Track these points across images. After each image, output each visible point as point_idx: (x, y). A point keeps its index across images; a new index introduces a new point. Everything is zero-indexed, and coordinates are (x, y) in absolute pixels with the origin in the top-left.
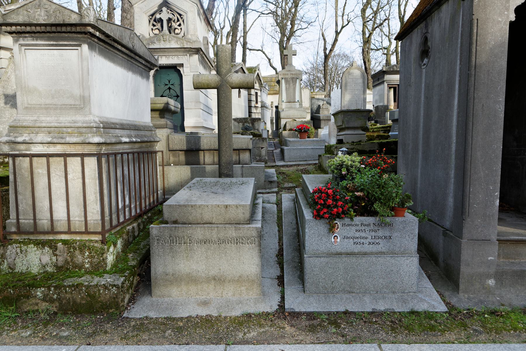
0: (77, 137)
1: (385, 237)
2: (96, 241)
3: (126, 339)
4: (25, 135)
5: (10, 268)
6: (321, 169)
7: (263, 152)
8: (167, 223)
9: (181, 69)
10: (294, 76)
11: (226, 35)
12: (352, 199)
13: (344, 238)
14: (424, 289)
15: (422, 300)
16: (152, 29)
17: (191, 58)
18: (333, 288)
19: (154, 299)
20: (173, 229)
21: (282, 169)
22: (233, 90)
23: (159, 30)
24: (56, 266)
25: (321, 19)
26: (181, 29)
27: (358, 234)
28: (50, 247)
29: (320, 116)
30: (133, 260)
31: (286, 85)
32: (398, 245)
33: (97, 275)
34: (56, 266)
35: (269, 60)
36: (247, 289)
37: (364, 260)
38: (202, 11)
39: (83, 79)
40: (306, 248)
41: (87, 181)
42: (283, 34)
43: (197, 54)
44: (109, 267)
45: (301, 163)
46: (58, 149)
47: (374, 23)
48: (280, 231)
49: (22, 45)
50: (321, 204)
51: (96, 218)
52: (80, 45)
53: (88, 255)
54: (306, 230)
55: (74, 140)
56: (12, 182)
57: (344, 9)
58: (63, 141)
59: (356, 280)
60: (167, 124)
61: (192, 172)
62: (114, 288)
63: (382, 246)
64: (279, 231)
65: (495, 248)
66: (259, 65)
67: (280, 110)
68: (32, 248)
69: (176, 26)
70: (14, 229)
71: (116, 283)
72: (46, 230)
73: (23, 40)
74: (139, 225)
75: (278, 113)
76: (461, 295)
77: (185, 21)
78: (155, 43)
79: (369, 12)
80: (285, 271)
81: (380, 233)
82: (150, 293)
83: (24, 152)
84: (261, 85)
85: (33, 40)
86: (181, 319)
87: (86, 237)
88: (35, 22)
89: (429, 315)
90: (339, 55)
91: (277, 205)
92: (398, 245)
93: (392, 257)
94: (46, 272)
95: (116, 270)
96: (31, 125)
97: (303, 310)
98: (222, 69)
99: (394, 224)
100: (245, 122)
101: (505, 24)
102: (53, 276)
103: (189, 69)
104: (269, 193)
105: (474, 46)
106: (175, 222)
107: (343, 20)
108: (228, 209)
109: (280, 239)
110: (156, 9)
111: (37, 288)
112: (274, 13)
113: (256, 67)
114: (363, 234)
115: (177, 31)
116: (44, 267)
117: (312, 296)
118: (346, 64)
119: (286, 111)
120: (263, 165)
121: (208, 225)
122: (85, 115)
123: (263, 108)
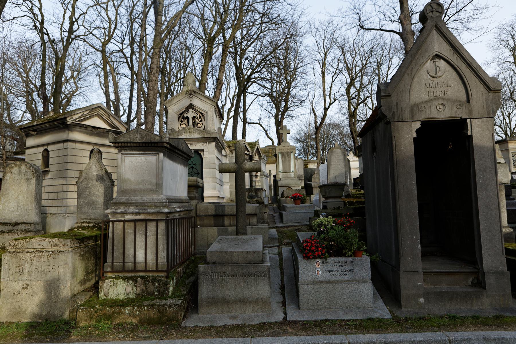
0: (154, 209)
1: (350, 270)
2: (163, 277)
3: (186, 337)
4: (122, 208)
5: (105, 295)
6: (311, 228)
7: (266, 216)
8: (209, 264)
9: (202, 153)
10: (288, 151)
11: (227, 111)
12: (328, 246)
13: (324, 271)
14: (378, 306)
15: (376, 312)
16: (181, 124)
17: (210, 145)
18: (318, 306)
19: (200, 315)
20: (214, 267)
21: (281, 229)
22: (246, 173)
23: (186, 125)
25: (311, 97)
26: (202, 124)
27: (332, 269)
28: (133, 281)
29: (312, 184)
30: (184, 290)
31: (282, 158)
32: (359, 276)
33: (163, 299)
35: (266, 131)
36: (261, 308)
37: (337, 286)
38: (217, 110)
39: (159, 173)
40: (300, 279)
41: (159, 237)
42: (278, 108)
43: (214, 142)
44: (170, 295)
45: (297, 224)
47: (358, 100)
48: (282, 273)
49: (123, 154)
50: (308, 250)
52: (158, 154)
54: (299, 267)
55: (153, 211)
57: (331, 90)
58: (146, 212)
59: (333, 300)
60: (195, 197)
61: (218, 232)
62: (176, 306)
63: (348, 276)
64: (281, 273)
65: (422, 277)
66: (258, 140)
67: (277, 179)
69: (199, 122)
70: (109, 269)
71: (177, 303)
72: (130, 269)
73: (124, 151)
74: (183, 269)
75: (275, 181)
76: (403, 309)
78: (183, 134)
79: (352, 90)
80: (286, 298)
81: (346, 268)
82: (197, 312)
84: (260, 156)
85: (130, 151)
86: (220, 327)
87: (156, 274)
89: (380, 321)
90: (329, 124)
91: (279, 256)
92: (359, 276)
93: (355, 283)
94: (129, 298)
95: (176, 295)
96: (125, 201)
97: (299, 319)
98: (239, 160)
99: (355, 262)
100: (250, 192)
101: (411, 139)
102: (134, 300)
103: (208, 153)
104: (272, 247)
105: (395, 151)
106: (214, 263)
107: (330, 99)
109: (282, 279)
110: (184, 110)
112: (270, 95)
113: (256, 142)
114: (336, 269)
115: (199, 125)
117: (305, 311)
118: (337, 132)
119: (283, 180)
120: (267, 226)
121: (236, 265)
122: (159, 195)
123: (262, 176)
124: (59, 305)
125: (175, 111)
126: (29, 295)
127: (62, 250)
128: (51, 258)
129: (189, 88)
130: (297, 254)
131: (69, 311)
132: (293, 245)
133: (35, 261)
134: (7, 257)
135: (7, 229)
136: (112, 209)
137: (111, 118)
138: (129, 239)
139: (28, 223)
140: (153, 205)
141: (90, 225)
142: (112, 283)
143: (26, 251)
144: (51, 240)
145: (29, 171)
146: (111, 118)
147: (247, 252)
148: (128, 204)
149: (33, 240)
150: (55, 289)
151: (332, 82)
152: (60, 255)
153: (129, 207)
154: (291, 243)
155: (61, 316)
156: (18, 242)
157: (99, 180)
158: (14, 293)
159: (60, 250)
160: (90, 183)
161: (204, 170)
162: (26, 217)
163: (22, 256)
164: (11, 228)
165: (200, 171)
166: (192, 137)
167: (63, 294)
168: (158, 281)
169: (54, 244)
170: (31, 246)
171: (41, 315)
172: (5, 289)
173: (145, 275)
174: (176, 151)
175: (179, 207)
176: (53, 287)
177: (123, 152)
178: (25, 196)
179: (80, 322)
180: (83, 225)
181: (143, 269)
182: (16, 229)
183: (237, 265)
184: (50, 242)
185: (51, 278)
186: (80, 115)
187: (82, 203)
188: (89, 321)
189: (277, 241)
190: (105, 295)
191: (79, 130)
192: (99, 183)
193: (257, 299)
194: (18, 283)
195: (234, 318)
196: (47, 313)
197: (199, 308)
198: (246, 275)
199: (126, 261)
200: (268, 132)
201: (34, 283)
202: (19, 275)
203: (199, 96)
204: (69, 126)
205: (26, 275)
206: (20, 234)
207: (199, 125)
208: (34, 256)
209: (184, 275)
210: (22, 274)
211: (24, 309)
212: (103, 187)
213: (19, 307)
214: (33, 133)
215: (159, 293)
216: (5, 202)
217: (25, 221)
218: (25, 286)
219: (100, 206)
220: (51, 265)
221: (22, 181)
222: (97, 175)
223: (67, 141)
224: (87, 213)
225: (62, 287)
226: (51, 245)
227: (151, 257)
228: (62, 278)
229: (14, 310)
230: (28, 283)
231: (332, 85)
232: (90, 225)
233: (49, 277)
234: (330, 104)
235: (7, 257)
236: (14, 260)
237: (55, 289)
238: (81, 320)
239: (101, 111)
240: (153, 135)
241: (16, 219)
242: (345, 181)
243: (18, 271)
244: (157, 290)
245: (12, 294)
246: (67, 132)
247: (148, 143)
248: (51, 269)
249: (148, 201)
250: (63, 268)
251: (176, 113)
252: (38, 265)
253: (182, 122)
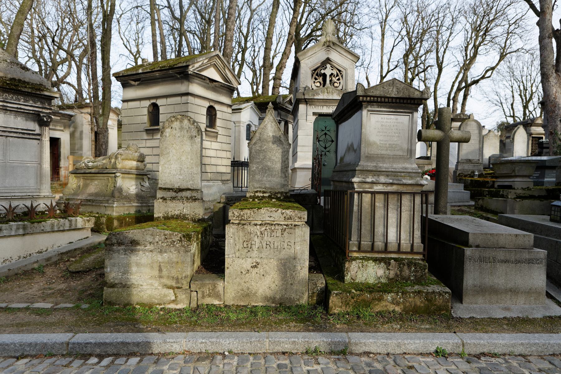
2: (419, 260)
4: (370, 177)
16: (314, 82)
20: (482, 251)
22: (451, 144)
23: (320, 83)
24: (388, 278)
26: (340, 83)
28: (385, 263)
34: (388, 278)
36: (535, 299)
46: (394, 188)
49: (369, 111)
51: (418, 242)
53: (413, 270)
56: (356, 212)
58: (402, 183)
62: (447, 294)
68: (371, 264)
69: (336, 81)
70: (355, 249)
72: (380, 250)
73: (371, 107)
77: (344, 76)
83: (366, 190)
85: (378, 107)
87: (410, 257)
88: (389, 96)
106: (478, 246)
108: (517, 237)
110: (319, 65)
111: (388, 293)
115: (336, 85)
116: (379, 278)
124: (295, 287)
125: (310, 65)
126: (260, 275)
127: (296, 223)
128: (285, 234)
129: (328, 39)
131: (307, 295)
133: (266, 235)
134: (231, 230)
135: (169, 196)
136: (358, 177)
137: (226, 70)
138: (380, 213)
139: (193, 190)
140: (407, 175)
141: (265, 195)
142: (360, 265)
143: (253, 223)
144: (284, 211)
145: (193, 126)
146: (226, 70)
148: (377, 172)
149: (263, 211)
150: (290, 269)
151: (394, 47)
152: (297, 230)
153: (378, 176)
155: (299, 300)
156: (244, 212)
157: (275, 142)
158: (242, 272)
159: (294, 223)
160: (265, 145)
162: (191, 182)
163: (249, 228)
164: (174, 194)
166: (330, 98)
167: (301, 275)
168: (415, 265)
169: (288, 216)
170: (260, 217)
171: (275, 298)
172: (230, 267)
173: (397, 257)
176: (288, 267)
177: (370, 109)
178: (189, 157)
179: (334, 308)
180: (257, 194)
181: (396, 250)
182: (180, 195)
183: (504, 249)
184: (283, 214)
185: (286, 257)
186: (200, 63)
187: (255, 168)
188: (344, 308)
190: (352, 279)
191: (197, 81)
192: (275, 145)
194: (246, 261)
195: (507, 309)
196: (282, 296)
197: (464, 297)
198: (519, 262)
199: (375, 240)
201: (265, 261)
202: (247, 251)
203: (339, 50)
204: (190, 76)
205: (256, 252)
206: (185, 202)
207: (336, 85)
208: (265, 229)
210: (250, 250)
211: (254, 291)
212: (280, 151)
213: (248, 289)
214: (133, 83)
215: (415, 278)
216: (165, 163)
217: (189, 187)
218: (254, 264)
219: (277, 173)
220: (286, 241)
221: (185, 138)
222: (273, 136)
223: (187, 94)
224: (262, 181)
225: (299, 267)
226: (285, 217)
227: (404, 236)
228: (299, 256)
229: (242, 292)
230: (258, 261)
231: (393, 49)
232: (265, 195)
233: (283, 254)
234: (388, 72)
235: (231, 230)
236: (241, 234)
237: (290, 269)
238: (335, 306)
239: (218, 60)
240: (412, 90)
241: (179, 184)
242: (478, 158)
243: (245, 246)
244: (414, 275)
245: (239, 273)
246: (186, 83)
247: (403, 99)
248: (286, 246)
249: (401, 170)
250: (301, 244)
251: (310, 69)
252: (270, 240)
253: (316, 79)
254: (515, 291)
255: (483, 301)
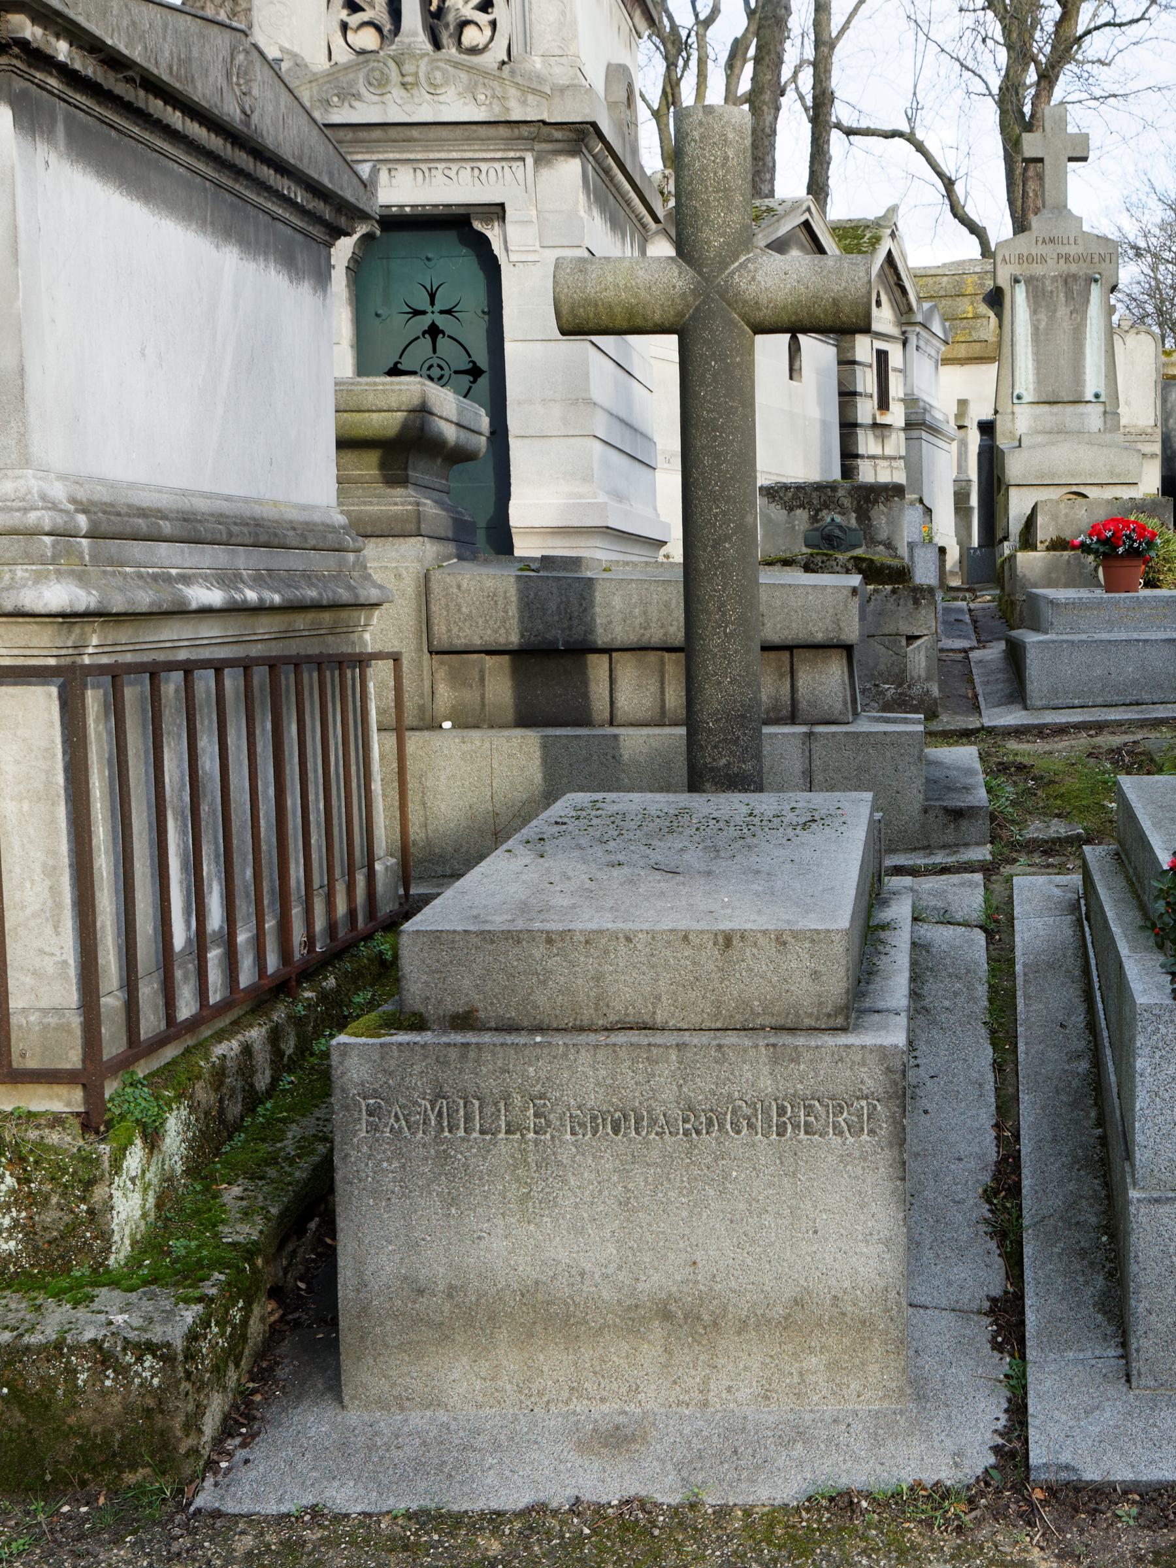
2: (57, 1121)
7: (918, 659)
8: (418, 1024)
9: (493, 233)
10: (1074, 268)
16: (344, 27)
17: (546, 173)
19: (353, 1416)
20: (453, 1054)
21: (1012, 745)
23: (379, 29)
26: (494, 24)
30: (246, 1214)
33: (58, 1295)
35: (949, 184)
42: (1020, 52)
43: (573, 153)
44: (118, 1257)
54: (1140, 1063)
62: (149, 1361)
66: (893, 209)
67: (1002, 442)
71: (157, 1334)
74: (275, 1037)
78: (357, 96)
82: (334, 1389)
84: (904, 312)
86: (495, 1519)
98: (706, 233)
100: (825, 506)
103: (533, 230)
104: (944, 870)
108: (734, 954)
113: (878, 224)
115: (471, 36)
119: (1033, 447)
120: (913, 725)
123: (915, 433)
130: (1124, 949)
132: (1094, 866)
147: (727, 940)
154: (1078, 841)
161: (509, 347)
165: (482, 360)
174: (156, 107)
175: (258, 581)
189: (982, 826)
193: (797, 1302)
200: (959, 188)
209: (288, 1080)
254: (691, 1317)
255: (478, 1385)
